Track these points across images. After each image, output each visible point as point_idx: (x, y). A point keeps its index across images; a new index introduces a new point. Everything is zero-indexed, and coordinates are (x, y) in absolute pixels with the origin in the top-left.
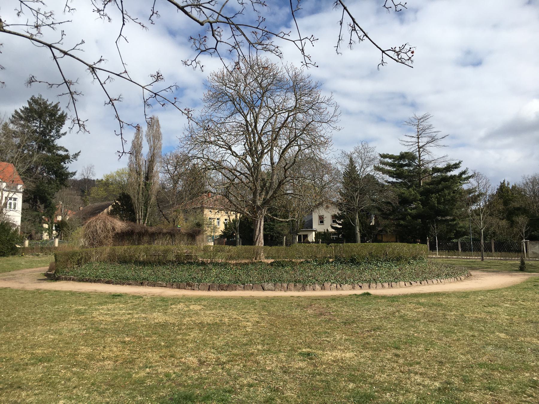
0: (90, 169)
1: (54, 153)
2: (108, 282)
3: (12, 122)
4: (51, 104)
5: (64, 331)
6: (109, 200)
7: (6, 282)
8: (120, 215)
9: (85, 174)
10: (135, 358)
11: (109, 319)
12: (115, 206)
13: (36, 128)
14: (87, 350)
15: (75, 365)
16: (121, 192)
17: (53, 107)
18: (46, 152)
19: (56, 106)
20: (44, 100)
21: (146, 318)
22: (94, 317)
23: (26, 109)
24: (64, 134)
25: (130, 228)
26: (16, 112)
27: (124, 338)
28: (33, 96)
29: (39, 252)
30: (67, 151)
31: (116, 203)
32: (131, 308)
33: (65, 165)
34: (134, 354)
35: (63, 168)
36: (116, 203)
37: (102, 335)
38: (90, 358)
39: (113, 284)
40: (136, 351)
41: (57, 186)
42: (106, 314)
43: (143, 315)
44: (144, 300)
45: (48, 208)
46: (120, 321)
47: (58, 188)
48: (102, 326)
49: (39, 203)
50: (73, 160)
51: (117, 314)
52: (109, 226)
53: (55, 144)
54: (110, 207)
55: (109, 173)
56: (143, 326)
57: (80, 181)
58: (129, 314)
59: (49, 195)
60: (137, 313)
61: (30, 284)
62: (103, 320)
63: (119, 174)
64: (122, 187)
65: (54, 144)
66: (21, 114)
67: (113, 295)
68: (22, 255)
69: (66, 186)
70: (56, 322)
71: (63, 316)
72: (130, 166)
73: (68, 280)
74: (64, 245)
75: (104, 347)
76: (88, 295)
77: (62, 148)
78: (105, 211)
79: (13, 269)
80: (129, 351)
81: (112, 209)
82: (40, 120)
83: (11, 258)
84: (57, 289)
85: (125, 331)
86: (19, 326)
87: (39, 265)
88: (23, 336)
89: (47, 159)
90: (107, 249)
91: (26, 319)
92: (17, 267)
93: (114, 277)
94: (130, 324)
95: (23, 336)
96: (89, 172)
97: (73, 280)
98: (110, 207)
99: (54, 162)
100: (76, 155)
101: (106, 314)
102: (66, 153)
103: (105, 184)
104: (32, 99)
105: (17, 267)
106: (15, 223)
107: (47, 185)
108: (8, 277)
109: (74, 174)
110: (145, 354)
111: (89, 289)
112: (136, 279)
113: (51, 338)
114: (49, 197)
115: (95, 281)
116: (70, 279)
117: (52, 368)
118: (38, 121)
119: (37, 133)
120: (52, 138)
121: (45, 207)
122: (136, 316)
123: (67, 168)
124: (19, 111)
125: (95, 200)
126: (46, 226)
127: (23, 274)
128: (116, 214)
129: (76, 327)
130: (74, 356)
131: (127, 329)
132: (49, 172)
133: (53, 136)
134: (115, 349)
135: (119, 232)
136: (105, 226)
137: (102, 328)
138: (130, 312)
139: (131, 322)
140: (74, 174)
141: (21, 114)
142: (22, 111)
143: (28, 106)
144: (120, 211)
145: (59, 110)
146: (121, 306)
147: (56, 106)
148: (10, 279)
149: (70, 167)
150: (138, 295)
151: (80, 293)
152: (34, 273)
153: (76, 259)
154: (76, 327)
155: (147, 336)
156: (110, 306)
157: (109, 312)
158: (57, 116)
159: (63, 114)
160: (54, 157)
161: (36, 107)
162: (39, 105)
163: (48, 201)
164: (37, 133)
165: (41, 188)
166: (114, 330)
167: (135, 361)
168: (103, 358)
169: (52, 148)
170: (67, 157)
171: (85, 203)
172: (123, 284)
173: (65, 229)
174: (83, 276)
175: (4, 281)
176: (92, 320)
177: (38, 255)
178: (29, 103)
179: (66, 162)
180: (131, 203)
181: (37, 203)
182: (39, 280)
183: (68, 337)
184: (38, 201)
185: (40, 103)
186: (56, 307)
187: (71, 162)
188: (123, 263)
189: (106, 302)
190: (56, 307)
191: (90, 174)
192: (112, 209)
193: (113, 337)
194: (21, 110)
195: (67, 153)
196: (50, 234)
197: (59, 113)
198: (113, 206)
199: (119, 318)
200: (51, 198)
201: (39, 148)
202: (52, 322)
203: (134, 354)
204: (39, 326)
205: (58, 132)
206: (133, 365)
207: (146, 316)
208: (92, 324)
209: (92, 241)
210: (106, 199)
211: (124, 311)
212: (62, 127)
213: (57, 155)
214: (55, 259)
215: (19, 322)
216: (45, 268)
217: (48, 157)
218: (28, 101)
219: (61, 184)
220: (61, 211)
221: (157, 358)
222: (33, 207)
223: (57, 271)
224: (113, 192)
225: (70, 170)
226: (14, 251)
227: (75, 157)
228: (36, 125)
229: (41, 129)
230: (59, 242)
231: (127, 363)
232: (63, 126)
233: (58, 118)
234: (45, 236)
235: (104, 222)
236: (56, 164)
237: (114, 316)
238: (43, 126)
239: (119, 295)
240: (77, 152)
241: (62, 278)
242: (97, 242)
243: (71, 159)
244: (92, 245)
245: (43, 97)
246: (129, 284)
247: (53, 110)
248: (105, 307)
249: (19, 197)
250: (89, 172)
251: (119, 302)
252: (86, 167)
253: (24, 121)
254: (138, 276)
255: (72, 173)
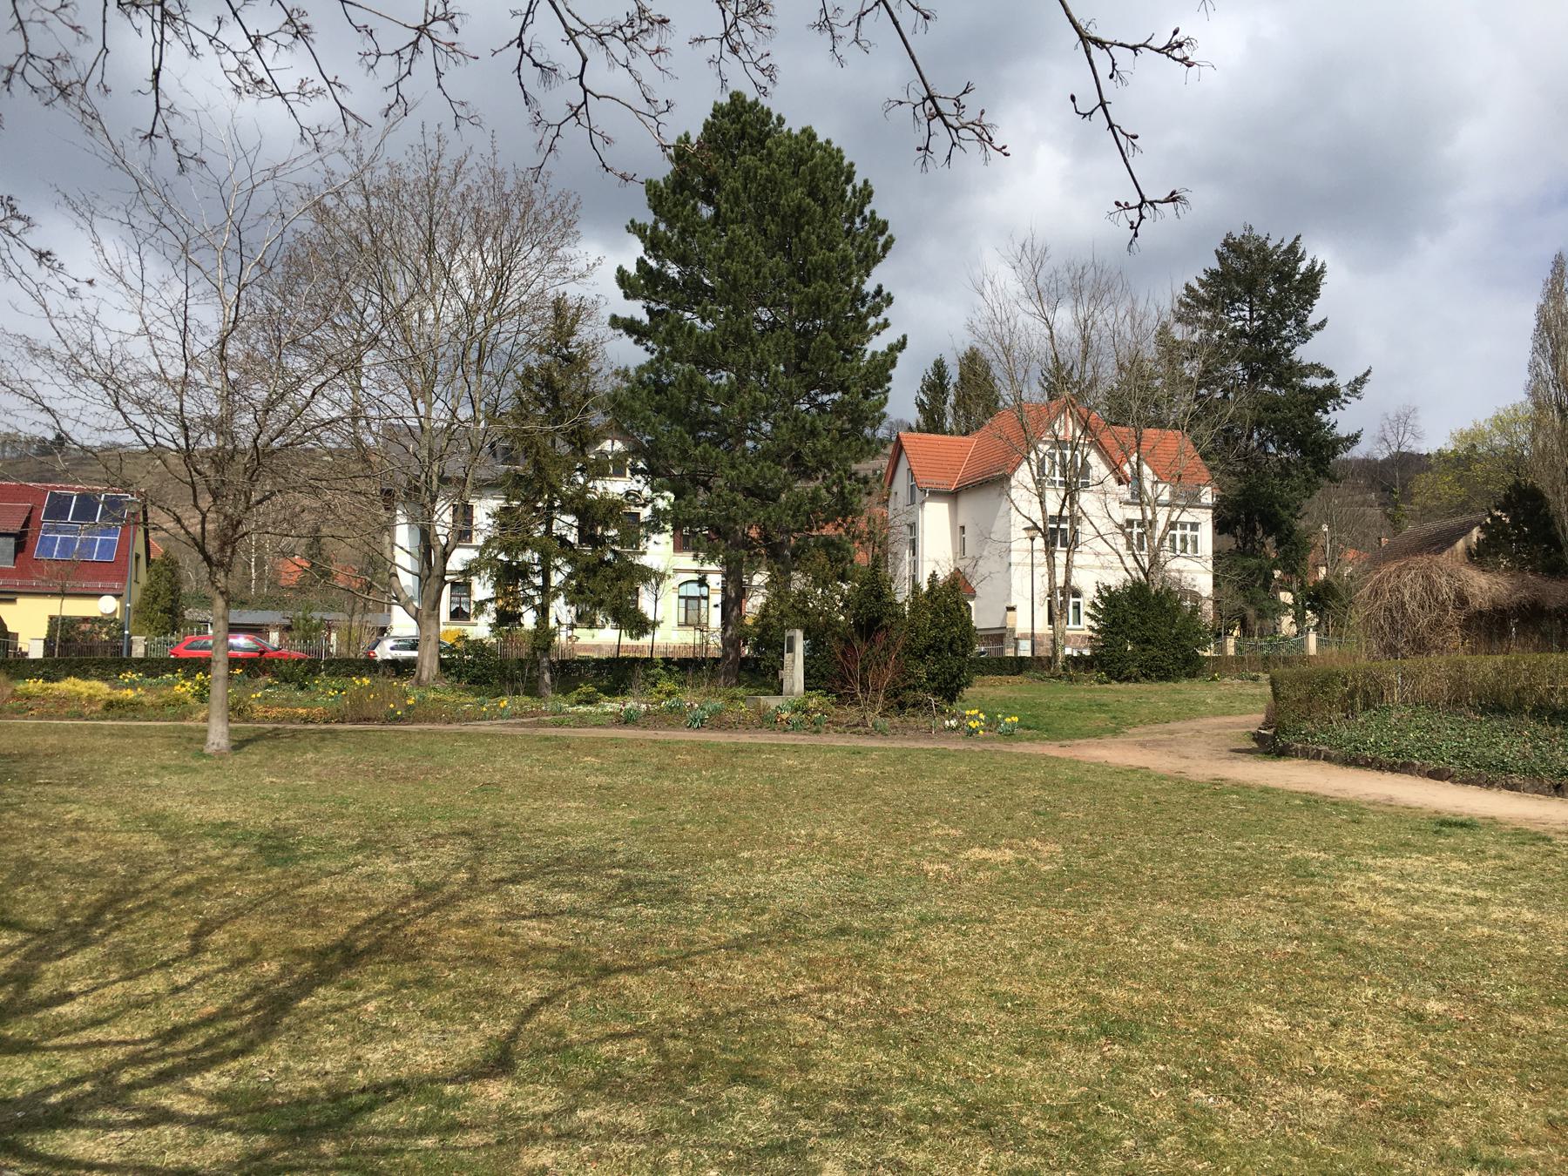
0: (1403, 420)
1: (1293, 387)
2: (1437, 775)
3: (1179, 320)
4: (1279, 246)
5: (1229, 935)
6: (1474, 511)
7: (1145, 751)
8: (1513, 557)
9: (1391, 437)
10: (1440, 1103)
11: (1390, 909)
12: (1492, 526)
13: (1241, 323)
14: (1268, 1021)
15: (1205, 1076)
16: (1510, 481)
17: (1285, 252)
18: (1272, 386)
19: (1292, 249)
20: (1258, 238)
21: (1535, 926)
22: (1342, 897)
23: (1213, 274)
24: (1320, 326)
25: (1525, 593)
26: (1188, 287)
27: (1425, 997)
28: (1229, 235)
29: (1258, 671)
30: (1329, 374)
31: (1493, 518)
32: (1488, 879)
33: (1325, 418)
34: (1444, 1078)
35: (1321, 426)
36: (1493, 518)
37: (1346, 969)
38: (1268, 1061)
39: (1454, 782)
40: (1455, 1068)
41: (1308, 480)
42: (1388, 892)
43: (1529, 916)
44: (1551, 854)
45: (1287, 547)
46: (1432, 925)
47: (1310, 487)
48: (1360, 935)
49: (1260, 533)
50: (1348, 399)
51: (1427, 897)
52: (1446, 591)
53: (1296, 358)
54: (1476, 533)
55: (1467, 426)
56: (1514, 959)
57: (1385, 462)
58: (1475, 901)
59: (1287, 507)
60: (1506, 903)
61: (1204, 763)
62: (1368, 913)
63: (1501, 424)
64: (1514, 462)
65: (1291, 361)
66: (1201, 291)
67: (1443, 823)
68: (1214, 679)
69: (1333, 479)
70: (1217, 896)
71: (1242, 878)
72: (1533, 393)
73: (1313, 758)
74: (1328, 651)
75: (1334, 1025)
76: (1356, 812)
77: (1315, 369)
78: (1460, 544)
79: (1178, 717)
80: (1425, 1063)
81: (1482, 536)
82: (1251, 302)
83: (1184, 684)
84: (1272, 784)
85: (1438, 970)
86: (1109, 892)
87: (1250, 707)
88: (1102, 928)
89: (1273, 406)
90: (1436, 668)
91: (1137, 872)
92: (1189, 711)
93: (1455, 758)
94: (1466, 944)
95: (1102, 928)
96: (1401, 430)
97: (1327, 758)
98: (1476, 533)
99: (1294, 411)
100: (1360, 381)
101: (1388, 892)
102: (1327, 381)
103: (1459, 462)
104: (1226, 244)
105: (1191, 709)
106: (1196, 589)
107: (1277, 481)
108: (1158, 737)
109: (1354, 439)
110: (1485, 1093)
111: (1369, 790)
112: (1533, 770)
113: (1177, 952)
114: (1285, 514)
115: (1393, 768)
116: (1317, 756)
117: (1129, 1071)
118: (1245, 301)
119: (1247, 336)
120: (1287, 345)
121: (1279, 543)
122: (1498, 913)
123: (1333, 426)
124: (1196, 285)
125: (1427, 513)
126: (1286, 597)
127: (1198, 731)
128: (1496, 554)
129: (1269, 923)
130: (1213, 1036)
131: (1447, 960)
132: (1284, 443)
133: (1288, 339)
134: (1369, 1040)
135: (1486, 606)
136: (1430, 588)
137: (1357, 944)
138: (1480, 893)
139: (1469, 935)
140: (1354, 439)
141: (1201, 291)
142: (1202, 284)
143: (1216, 266)
144: (1511, 542)
145: (1302, 259)
146: (1455, 865)
147: (1292, 249)
148: (1157, 744)
149: (1341, 420)
150: (1540, 828)
151: (1335, 804)
152: (1229, 731)
153: (1340, 690)
154: (1269, 923)
155: (1520, 1008)
156: (1414, 863)
157: (1400, 886)
158: (1298, 277)
159: (1314, 268)
160: (1296, 396)
161: (1238, 264)
162: (1248, 258)
163: (1284, 527)
164: (1247, 336)
165: (1263, 490)
166: (1397, 960)
167: (1435, 1114)
168: (1315, 1068)
169: (1287, 372)
170: (1331, 393)
171: (1395, 523)
172: (1490, 784)
173: (1332, 603)
174: (1357, 749)
175: (1139, 748)
176: (1333, 907)
177: (1255, 679)
178: (1220, 256)
179: (1329, 409)
180: (1546, 514)
181: (1255, 534)
182: (1233, 751)
183: (1232, 956)
184: (1258, 526)
185: (1250, 251)
186: (1238, 843)
187: (1344, 405)
188: (1493, 711)
189: (1406, 845)
190: (1238, 843)
191: (1407, 436)
192: (1482, 536)
193: (1385, 985)
194: (1199, 280)
195: (1332, 379)
196: (1299, 619)
197: (1303, 266)
198: (1484, 528)
199: (1430, 911)
200: (1292, 515)
201: (1253, 377)
202: (1204, 894)
203: (1444, 1078)
204: (1161, 899)
205: (1301, 322)
206: (1421, 1133)
207: (1539, 918)
208: (1328, 922)
209: (1389, 638)
210: (1464, 507)
211: (1455, 889)
212: (1312, 305)
213: (1303, 390)
214: (1273, 690)
215: (1114, 881)
216: (1255, 719)
217: (1277, 400)
218: (1217, 251)
219: (1317, 473)
220: (1325, 552)
221: (1538, 1127)
222: (1245, 545)
223: (1280, 729)
224: (1486, 483)
225: (1343, 430)
226: (1191, 667)
227: (1355, 390)
228: (1242, 314)
229: (1256, 323)
230: (1319, 641)
231: (1399, 1118)
232: (1315, 302)
233: (1300, 281)
234: (1287, 625)
235: (1428, 577)
236: (1300, 416)
237: (1415, 901)
238: (1259, 315)
239: (1467, 825)
240: (1360, 374)
241: (1296, 750)
242: (1408, 642)
243: (1343, 397)
244: (1391, 650)
245: (1255, 233)
246: (1512, 788)
247: (1284, 263)
248: (1394, 863)
249: (1205, 519)
250: (1401, 430)
251: (1454, 850)
252: (1392, 416)
253: (1208, 310)
254: (1543, 760)
255: (1348, 439)
